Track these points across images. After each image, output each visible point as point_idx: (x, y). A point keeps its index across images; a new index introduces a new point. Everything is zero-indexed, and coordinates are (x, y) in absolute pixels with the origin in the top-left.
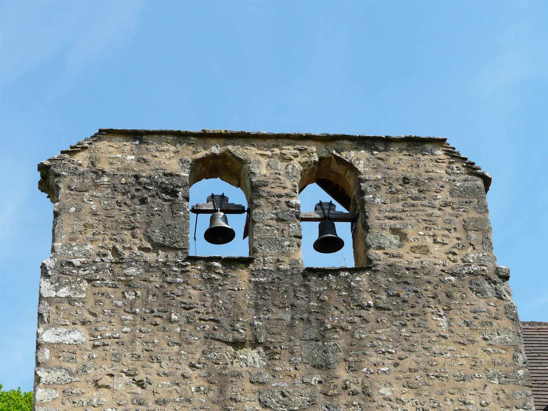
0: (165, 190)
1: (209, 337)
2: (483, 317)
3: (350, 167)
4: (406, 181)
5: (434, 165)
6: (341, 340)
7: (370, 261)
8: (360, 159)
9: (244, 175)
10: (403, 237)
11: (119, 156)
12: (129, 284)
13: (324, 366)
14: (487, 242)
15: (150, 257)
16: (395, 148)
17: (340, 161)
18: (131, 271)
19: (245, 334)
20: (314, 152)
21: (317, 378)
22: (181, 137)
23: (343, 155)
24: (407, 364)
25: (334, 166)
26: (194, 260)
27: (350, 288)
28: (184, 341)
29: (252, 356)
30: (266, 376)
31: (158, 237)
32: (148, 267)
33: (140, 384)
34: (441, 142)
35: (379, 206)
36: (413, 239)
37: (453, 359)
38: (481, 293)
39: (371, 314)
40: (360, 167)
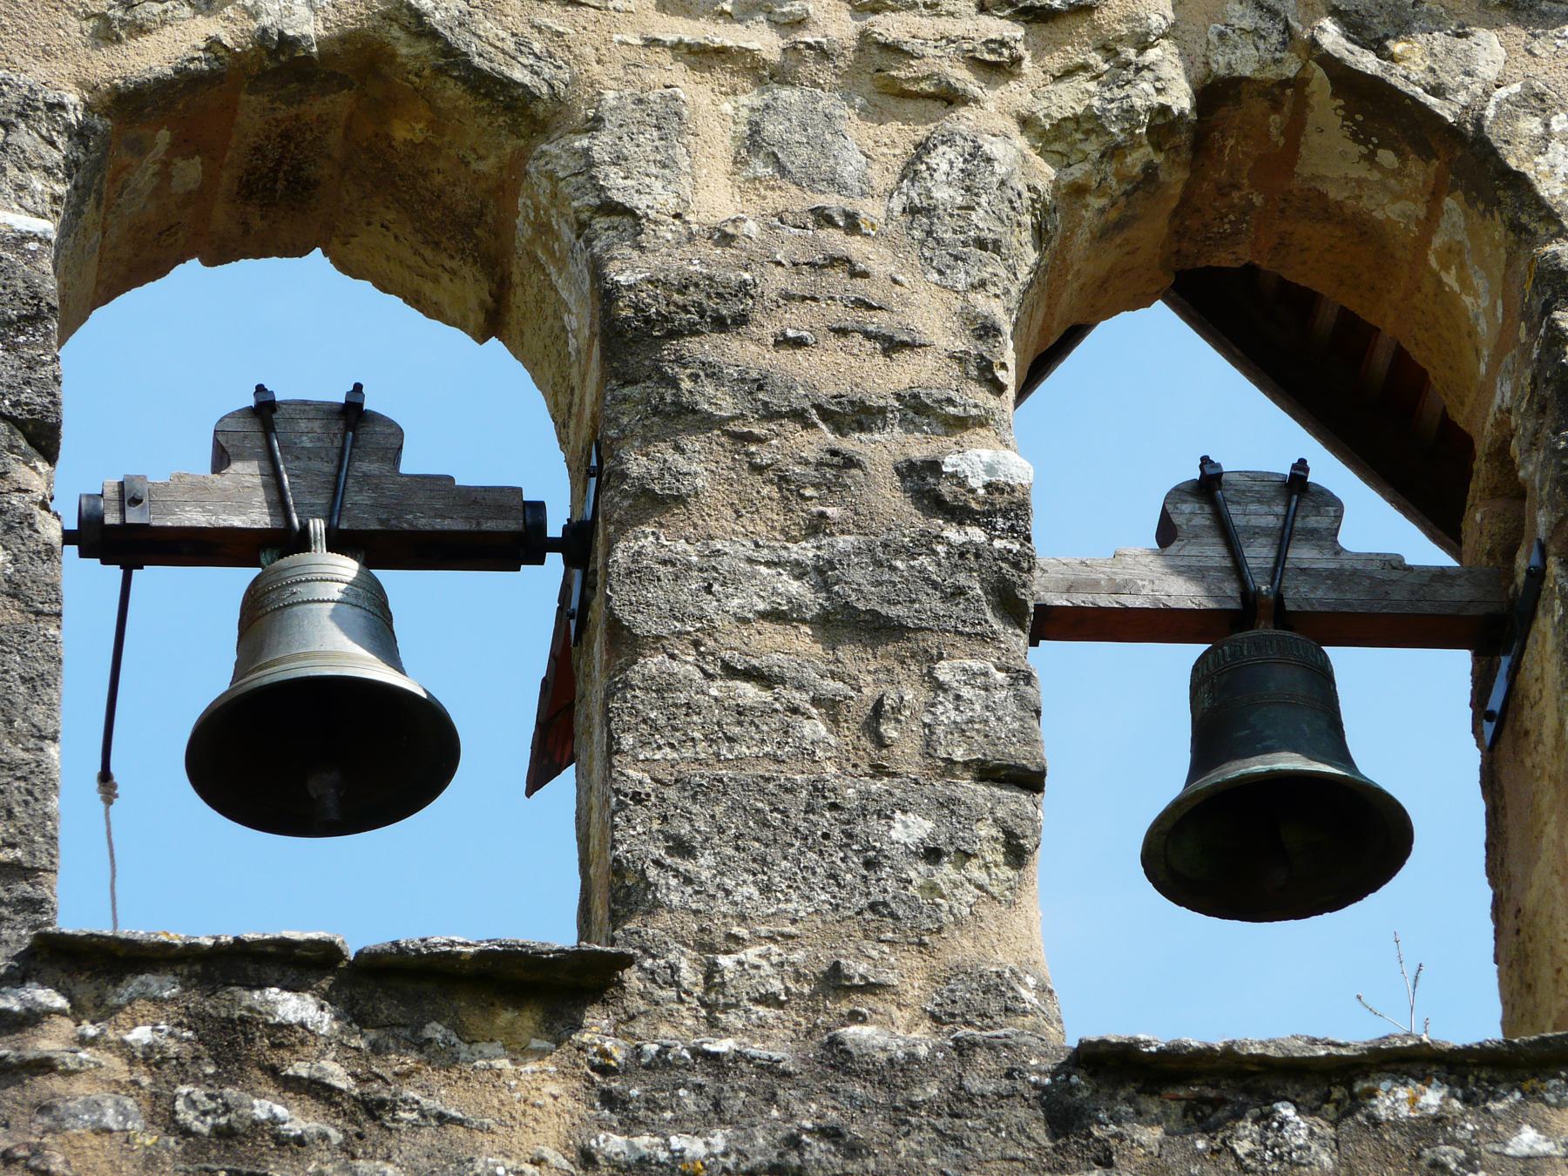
23: (1412, 64)
25: (1332, 156)
26: (97, 966)
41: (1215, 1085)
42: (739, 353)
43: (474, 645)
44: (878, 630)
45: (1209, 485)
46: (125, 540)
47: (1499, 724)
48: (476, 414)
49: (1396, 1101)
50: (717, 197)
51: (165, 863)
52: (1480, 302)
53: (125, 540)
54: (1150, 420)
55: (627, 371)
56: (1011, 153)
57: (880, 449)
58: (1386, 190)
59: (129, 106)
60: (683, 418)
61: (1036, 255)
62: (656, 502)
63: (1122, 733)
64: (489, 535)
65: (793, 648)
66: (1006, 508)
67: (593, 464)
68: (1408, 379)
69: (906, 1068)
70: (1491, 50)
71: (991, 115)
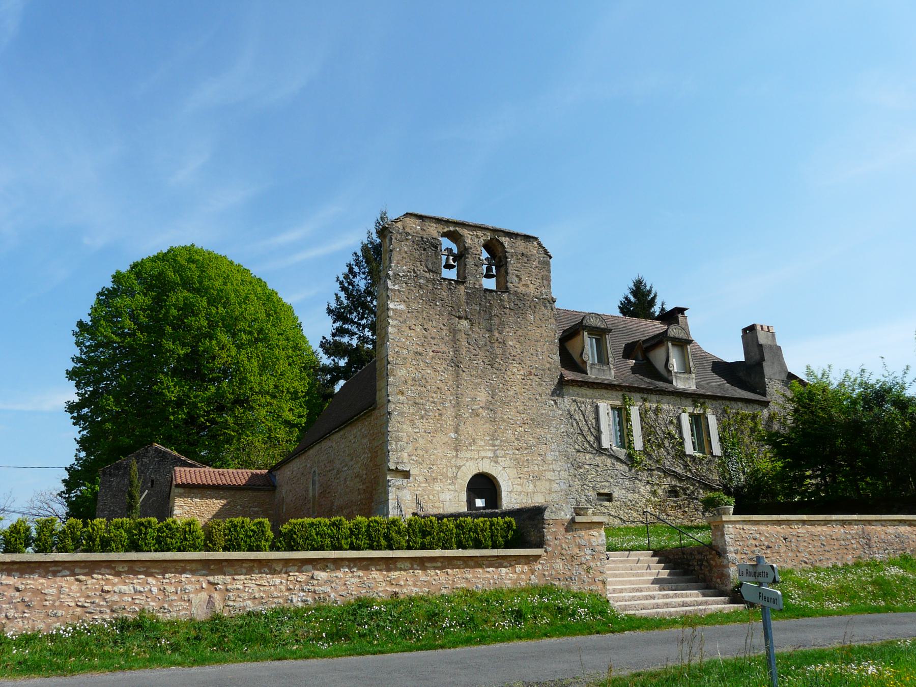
0: (433, 246)
1: (450, 314)
2: (546, 317)
3: (502, 244)
4: (523, 254)
5: (532, 248)
6: (496, 321)
7: (507, 288)
8: (505, 241)
9: (645, 400)
10: (520, 279)
11: (414, 225)
12: (421, 287)
13: (490, 330)
14: (549, 286)
15: (427, 275)
16: (519, 239)
17: (498, 240)
18: (421, 281)
19: (462, 314)
20: (489, 236)
21: (487, 335)
22: (438, 221)
23: (500, 239)
24: (519, 333)
25: (494, 241)
26: (445, 279)
27: (501, 299)
28: (441, 314)
29: (465, 323)
30: (470, 333)
31: (430, 267)
32: (428, 280)
33: (425, 330)
34: (536, 239)
35: (513, 264)
36: (523, 281)
37: (535, 333)
38: (546, 307)
39: (507, 311)
40: (506, 245)
58: (497, 244)
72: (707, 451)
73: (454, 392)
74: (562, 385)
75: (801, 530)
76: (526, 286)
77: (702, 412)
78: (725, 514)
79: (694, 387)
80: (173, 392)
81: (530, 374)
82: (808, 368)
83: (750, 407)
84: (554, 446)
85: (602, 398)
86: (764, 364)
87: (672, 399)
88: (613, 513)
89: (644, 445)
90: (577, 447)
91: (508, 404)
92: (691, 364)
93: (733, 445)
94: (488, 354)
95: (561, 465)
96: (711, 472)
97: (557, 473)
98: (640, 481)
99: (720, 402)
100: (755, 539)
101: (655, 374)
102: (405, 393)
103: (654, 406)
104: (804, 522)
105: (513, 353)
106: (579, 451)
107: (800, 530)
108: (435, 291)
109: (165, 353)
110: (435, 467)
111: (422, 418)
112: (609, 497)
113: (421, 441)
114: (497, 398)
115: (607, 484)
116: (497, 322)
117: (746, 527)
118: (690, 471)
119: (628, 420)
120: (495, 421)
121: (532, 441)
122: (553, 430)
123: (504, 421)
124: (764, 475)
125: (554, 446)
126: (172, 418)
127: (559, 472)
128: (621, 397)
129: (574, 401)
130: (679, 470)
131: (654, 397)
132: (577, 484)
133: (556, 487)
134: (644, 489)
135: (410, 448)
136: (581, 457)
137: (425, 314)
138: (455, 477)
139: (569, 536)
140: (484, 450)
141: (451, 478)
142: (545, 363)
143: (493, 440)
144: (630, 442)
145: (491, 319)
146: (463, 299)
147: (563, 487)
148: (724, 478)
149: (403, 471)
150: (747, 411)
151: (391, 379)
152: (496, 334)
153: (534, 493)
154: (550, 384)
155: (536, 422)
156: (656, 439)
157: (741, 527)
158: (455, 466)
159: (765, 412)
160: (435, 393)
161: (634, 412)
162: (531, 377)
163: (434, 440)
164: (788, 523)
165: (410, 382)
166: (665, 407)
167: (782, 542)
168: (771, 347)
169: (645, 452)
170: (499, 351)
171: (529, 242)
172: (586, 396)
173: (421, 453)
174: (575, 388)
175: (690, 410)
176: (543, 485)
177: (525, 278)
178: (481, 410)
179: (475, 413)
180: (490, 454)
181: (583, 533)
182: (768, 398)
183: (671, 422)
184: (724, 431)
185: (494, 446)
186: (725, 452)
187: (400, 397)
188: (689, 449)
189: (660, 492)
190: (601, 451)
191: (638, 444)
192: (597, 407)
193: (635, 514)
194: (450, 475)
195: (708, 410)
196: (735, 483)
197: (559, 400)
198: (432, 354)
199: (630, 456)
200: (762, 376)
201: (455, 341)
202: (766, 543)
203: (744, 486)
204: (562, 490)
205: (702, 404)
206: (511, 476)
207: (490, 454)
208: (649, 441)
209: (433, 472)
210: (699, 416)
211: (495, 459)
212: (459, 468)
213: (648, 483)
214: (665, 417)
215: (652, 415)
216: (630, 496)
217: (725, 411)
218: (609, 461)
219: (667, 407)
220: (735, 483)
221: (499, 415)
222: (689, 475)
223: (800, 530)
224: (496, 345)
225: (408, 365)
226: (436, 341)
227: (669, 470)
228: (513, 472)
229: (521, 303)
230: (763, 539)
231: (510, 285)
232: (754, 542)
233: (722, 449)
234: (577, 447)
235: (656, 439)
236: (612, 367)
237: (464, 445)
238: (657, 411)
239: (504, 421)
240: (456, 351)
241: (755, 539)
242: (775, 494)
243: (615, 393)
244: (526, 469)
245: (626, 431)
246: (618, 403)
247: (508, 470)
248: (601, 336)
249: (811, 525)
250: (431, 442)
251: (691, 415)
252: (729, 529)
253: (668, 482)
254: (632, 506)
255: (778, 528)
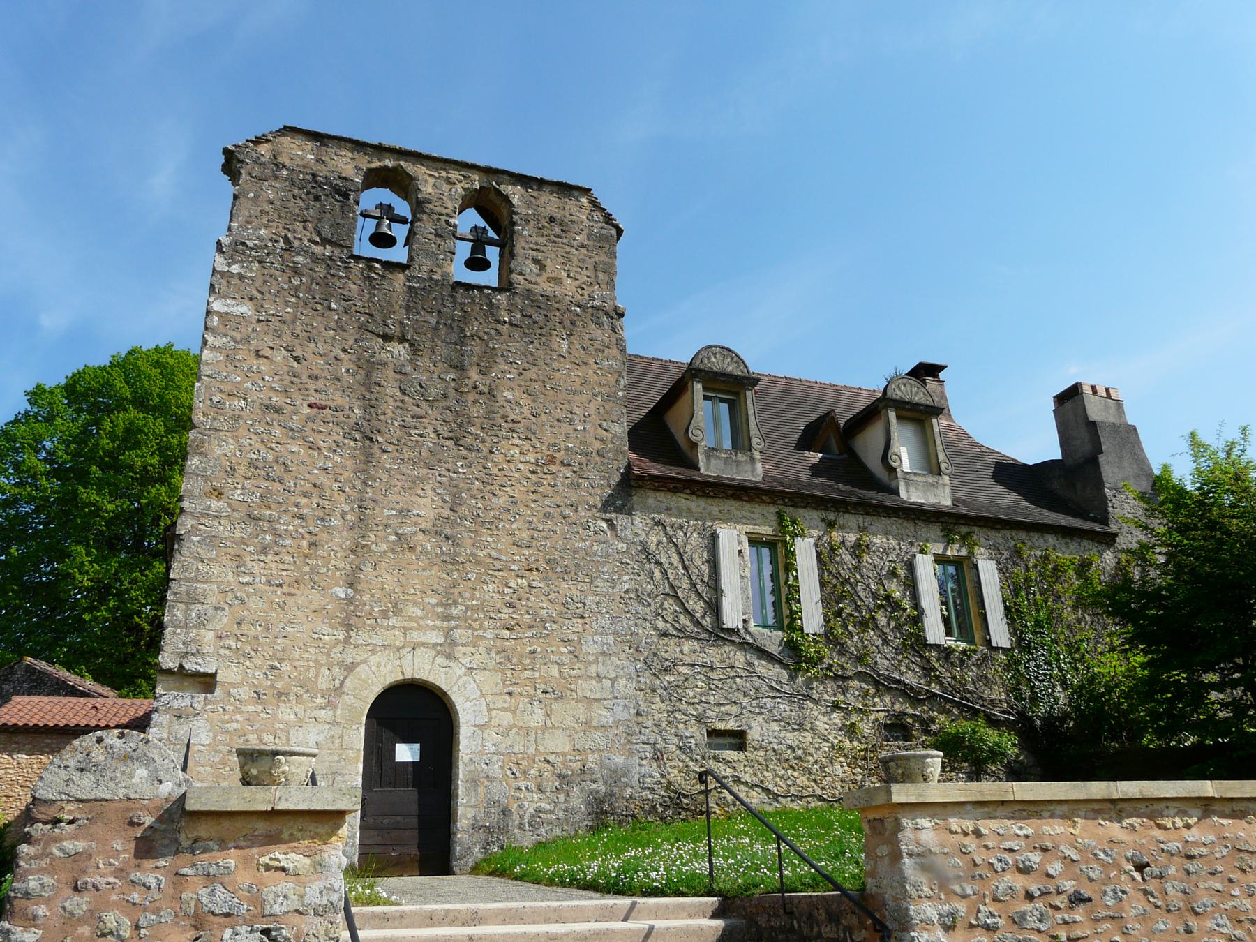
0: (338, 192)
1: (362, 328)
2: (598, 345)
3: (506, 199)
4: (552, 219)
5: (577, 210)
6: (476, 347)
7: (511, 284)
8: (516, 194)
9: (831, 525)
11: (301, 153)
12: (296, 271)
13: (459, 367)
14: (611, 283)
15: (318, 249)
16: (547, 190)
17: (498, 192)
18: (300, 259)
19: (393, 329)
20: (476, 182)
21: (451, 376)
22: (358, 146)
23: (502, 188)
24: (531, 374)
25: (492, 196)
26: (358, 258)
27: (490, 304)
28: (339, 328)
30: (409, 369)
31: (327, 232)
32: (315, 258)
33: (297, 359)
34: (586, 191)
35: (525, 236)
36: (555, 274)
37: (569, 376)
38: (599, 324)
39: (505, 329)
40: (515, 201)
41: (469, 287)
42: (430, 206)
43: (400, 232)
44: (441, 236)
45: (476, 227)
46: (365, 215)
47: (501, 255)
48: (402, 208)
49: (486, 291)
50: (430, 190)
51: (365, 248)
52: (505, 213)
53: (365, 215)
54: (471, 219)
55: (418, 206)
56: (460, 190)
57: (443, 218)
58: (498, 201)
59: (370, 170)
60: (424, 212)
61: (17, 699)
62: (420, 220)
63: (464, 250)
64: (403, 221)
65: (432, 237)
66: (455, 226)
67: (414, 215)
68: (497, 219)
69: (437, 281)
70: (510, 188)
71: (459, 187)
72: (977, 637)
73: (354, 495)
74: (627, 492)
75: (1200, 833)
76: (558, 281)
77: (964, 553)
78: (906, 777)
79: (948, 503)
80: (87, 573)
81: (552, 460)
82: (1193, 435)
83: (1074, 546)
84: (604, 621)
85: (728, 519)
86: (1101, 458)
87: (895, 524)
88: (747, 778)
89: (827, 621)
90: (661, 624)
91: (491, 525)
92: (941, 456)
93: (1038, 623)
94: (449, 416)
95: (620, 664)
96: (988, 683)
97: (607, 683)
98: (817, 702)
99: (1007, 533)
100: (1025, 870)
101: (867, 479)
102: (227, 493)
103: (852, 538)
104: (1207, 806)
105: (512, 417)
106: (665, 634)
107: (1193, 835)
108: (331, 280)
109: (83, 508)
110: (285, 667)
111: (264, 551)
112: (738, 739)
113: (254, 604)
114: (463, 510)
115: (734, 709)
116: (477, 350)
117: (987, 826)
118: (938, 680)
119: (790, 567)
120: (454, 562)
121: (546, 609)
122: (602, 586)
123: (477, 562)
124: (1109, 689)
125: (604, 621)
126: (87, 617)
127: (614, 680)
128: (773, 517)
129: (658, 523)
130: (912, 678)
131: (852, 520)
132: (658, 709)
133: (602, 715)
134: (827, 723)
135: (224, 620)
136: (671, 648)
137: (299, 327)
138: (339, 691)
139: (152, 874)
140: (419, 628)
141: (327, 693)
142: (590, 439)
143: (446, 605)
144: (794, 616)
145: (462, 343)
146: (400, 299)
147: (622, 715)
148: (1020, 697)
149: (197, 675)
150: (1065, 554)
151: (193, 462)
152: (474, 374)
153: (544, 729)
154: (600, 485)
155: (556, 568)
156: (857, 609)
157: (969, 825)
158: (341, 664)
159: (1109, 556)
160: (305, 495)
161: (805, 552)
162: (554, 469)
163: (291, 602)
164: (1151, 808)
165: (242, 470)
166: (879, 541)
167: (1128, 881)
168: (1114, 428)
169: (828, 635)
170: (475, 411)
171: (570, 197)
172: (689, 514)
173: (252, 631)
174: (661, 496)
175: (938, 548)
176: (569, 713)
177: (554, 267)
178: (420, 536)
179: (405, 544)
180: (436, 638)
181: (231, 859)
182: (1114, 527)
183: (893, 574)
184: (1016, 593)
185: (447, 618)
186: (1020, 640)
187: (214, 504)
188: (934, 631)
189: (865, 728)
190: (719, 634)
191: (812, 618)
192: (714, 538)
193: (802, 780)
194: (323, 684)
195: (977, 550)
196: (1043, 708)
197: (621, 521)
198: (306, 410)
199: (791, 647)
200: (1099, 483)
201: (369, 384)
202: (1069, 886)
203: (1065, 716)
204: (617, 723)
205: (964, 538)
206: (486, 688)
207: (436, 638)
208: (838, 613)
209: (280, 677)
210: (958, 562)
211: (448, 650)
212: (350, 668)
213: (836, 706)
214: (877, 561)
215: (847, 558)
216: (792, 738)
217: (1017, 552)
218: (739, 658)
219: (884, 541)
220: (1043, 708)
221: (467, 548)
222: (935, 689)
223: (1193, 835)
224: (472, 396)
225: (243, 432)
226: (320, 385)
227: (888, 678)
228: (492, 681)
229: (538, 316)
230: (1055, 868)
231: (516, 278)
232: (1020, 882)
233: (1013, 632)
234: (661, 624)
235: (857, 609)
236: (757, 455)
237: (369, 615)
238: (858, 550)
239: (477, 562)
240: (370, 407)
241: (1025, 870)
242: (1137, 731)
243: (758, 509)
244: (528, 674)
245: (784, 590)
246: (767, 530)
247: (479, 676)
248: (737, 394)
249: (1233, 815)
250: (281, 607)
251: (940, 560)
252: (922, 834)
253: (885, 704)
254: (797, 760)
255: (1114, 829)
